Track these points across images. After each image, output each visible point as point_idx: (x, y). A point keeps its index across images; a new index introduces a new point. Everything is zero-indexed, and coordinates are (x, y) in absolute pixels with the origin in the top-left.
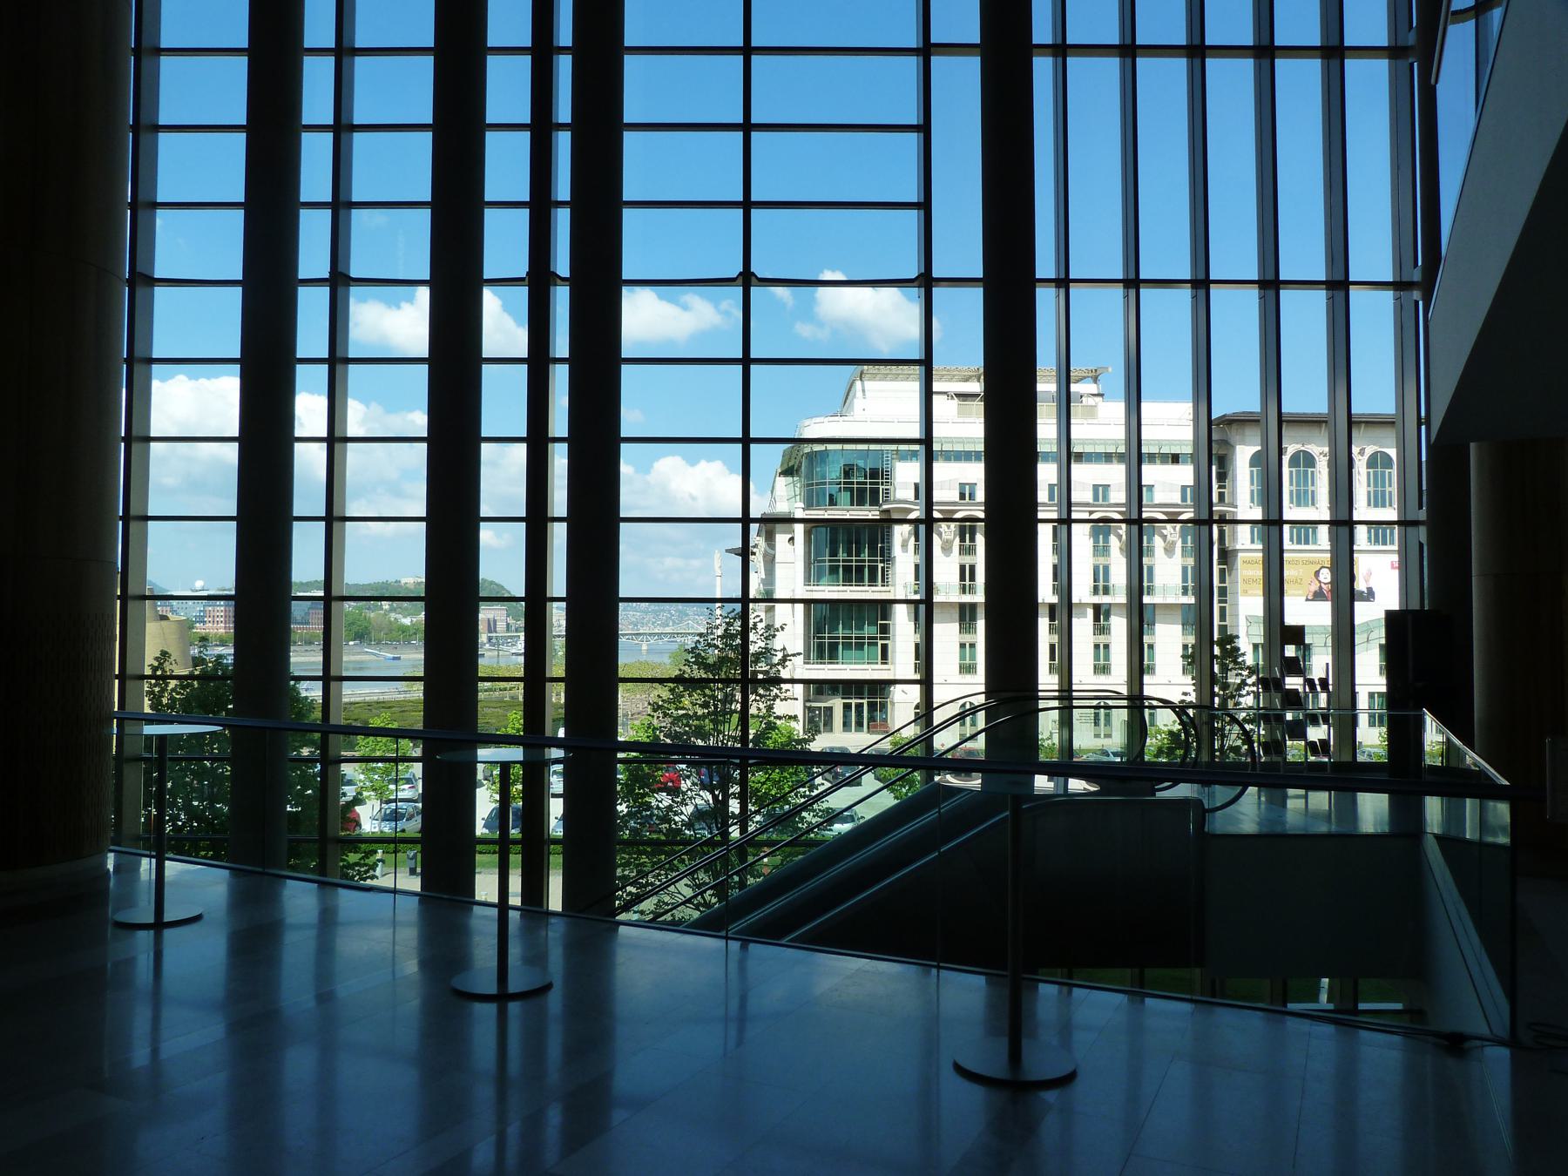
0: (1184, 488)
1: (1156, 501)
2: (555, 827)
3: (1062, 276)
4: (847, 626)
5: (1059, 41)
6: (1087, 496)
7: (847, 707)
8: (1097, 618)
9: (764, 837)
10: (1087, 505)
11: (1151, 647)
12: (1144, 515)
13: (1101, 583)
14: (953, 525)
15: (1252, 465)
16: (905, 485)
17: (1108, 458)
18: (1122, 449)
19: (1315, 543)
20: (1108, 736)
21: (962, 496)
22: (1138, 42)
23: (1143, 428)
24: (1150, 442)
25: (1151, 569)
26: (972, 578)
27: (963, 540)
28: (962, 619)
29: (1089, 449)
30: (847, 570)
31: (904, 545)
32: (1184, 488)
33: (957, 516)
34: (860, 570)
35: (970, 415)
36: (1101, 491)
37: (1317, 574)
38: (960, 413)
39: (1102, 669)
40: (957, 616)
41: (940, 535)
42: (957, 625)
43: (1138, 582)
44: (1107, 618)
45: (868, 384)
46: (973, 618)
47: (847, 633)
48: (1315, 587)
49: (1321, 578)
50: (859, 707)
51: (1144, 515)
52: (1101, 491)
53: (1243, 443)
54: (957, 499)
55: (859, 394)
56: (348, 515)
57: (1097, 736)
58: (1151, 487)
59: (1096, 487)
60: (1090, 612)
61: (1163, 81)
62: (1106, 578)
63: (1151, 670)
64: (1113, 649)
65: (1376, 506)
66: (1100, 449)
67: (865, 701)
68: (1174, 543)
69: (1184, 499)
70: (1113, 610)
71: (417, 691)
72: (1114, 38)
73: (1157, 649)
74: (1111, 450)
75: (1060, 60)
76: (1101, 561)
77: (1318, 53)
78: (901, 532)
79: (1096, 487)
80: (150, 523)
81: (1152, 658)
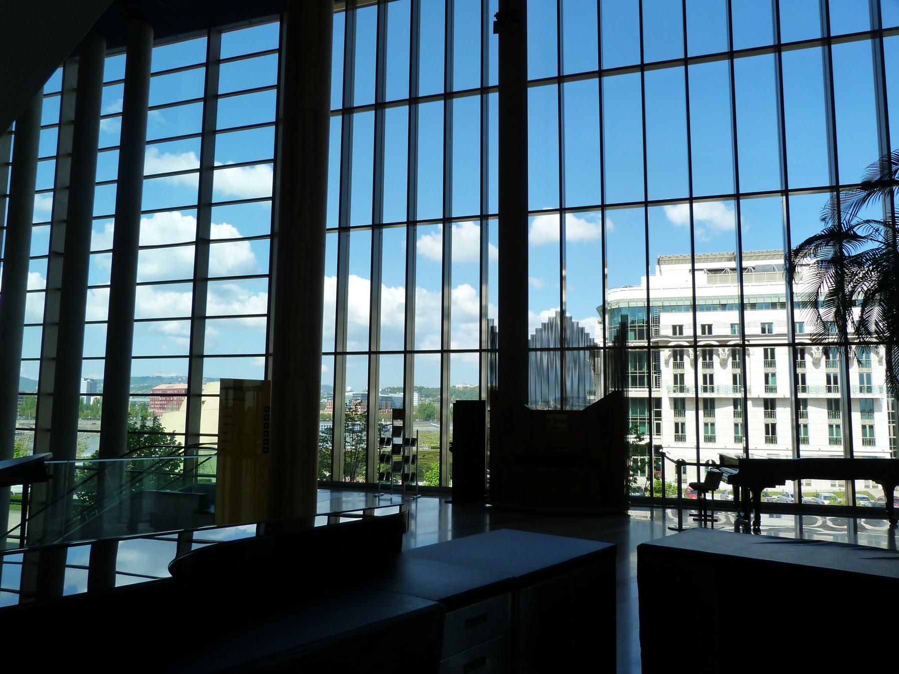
0: (732, 326)
3: (834, 184)
5: (826, 36)
6: (670, 332)
11: (805, 426)
12: (797, 341)
13: (866, 385)
14: (726, 349)
16: (666, 327)
17: (773, 305)
18: (783, 300)
21: (763, 331)
22: (884, 27)
23: (651, 291)
24: (702, 298)
25: (803, 376)
26: (836, 382)
27: (675, 359)
28: (766, 407)
29: (760, 301)
31: (667, 363)
32: (732, 326)
33: (729, 343)
34: (642, 378)
35: (775, 280)
36: (766, 329)
38: (709, 281)
39: (869, 441)
41: (718, 355)
42: (826, 411)
43: (798, 381)
44: (805, 407)
45: (663, 267)
46: (837, 409)
47: (634, 416)
51: (797, 341)
52: (678, 330)
54: (759, 332)
55: (658, 272)
56: (416, 349)
58: (801, 324)
59: (674, 327)
61: (804, 66)
62: (712, 382)
63: (806, 441)
64: (687, 426)
68: (819, 360)
69: (734, 331)
70: (809, 403)
71: (215, 440)
72: (818, 35)
73: (810, 428)
74: (775, 300)
75: (826, 47)
76: (679, 371)
77: (484, 96)
78: (665, 354)
79: (674, 327)
80: (381, 356)
81: (806, 433)
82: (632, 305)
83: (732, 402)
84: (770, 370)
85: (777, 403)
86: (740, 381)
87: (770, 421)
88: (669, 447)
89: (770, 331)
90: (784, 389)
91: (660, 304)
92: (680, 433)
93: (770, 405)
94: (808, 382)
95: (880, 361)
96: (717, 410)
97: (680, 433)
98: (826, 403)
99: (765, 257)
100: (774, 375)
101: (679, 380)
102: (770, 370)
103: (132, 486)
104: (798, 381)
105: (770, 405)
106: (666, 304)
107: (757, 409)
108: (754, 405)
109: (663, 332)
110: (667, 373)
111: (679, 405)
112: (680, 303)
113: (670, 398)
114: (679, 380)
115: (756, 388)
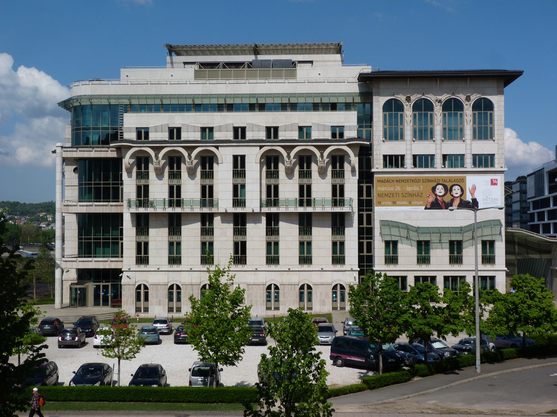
1: (313, 138)
2: (439, 388)
4: (97, 231)
6: (133, 136)
7: (97, 289)
8: (268, 223)
9: (215, 383)
10: (262, 141)
15: (384, 111)
17: (348, 106)
19: (432, 166)
20: (277, 308)
28: (236, 224)
30: (98, 190)
37: (434, 189)
40: (330, 223)
42: (297, 226)
43: (272, 194)
44: (277, 223)
48: (431, 199)
49: (454, 192)
50: (106, 287)
53: (379, 95)
57: (268, 308)
60: (264, 219)
62: (179, 195)
65: (480, 138)
66: (214, 101)
67: (109, 284)
70: (281, 217)
74: (350, 100)
82: (95, 102)
83: (199, 218)
84: (239, 181)
85: (248, 219)
86: (207, 193)
87: (240, 238)
88: (129, 270)
89: (341, 135)
90: (253, 202)
91: (126, 102)
92: (143, 255)
93: (240, 221)
94: (314, 195)
95: (353, 170)
96: (183, 228)
97: (143, 255)
98: (297, 218)
99: (235, 52)
100: (243, 186)
101: (143, 192)
102: (239, 181)
103: (432, 314)
104: (272, 194)
105: (240, 221)
106: (166, 102)
107: (226, 225)
108: (223, 221)
109: (126, 136)
110: (129, 186)
111: (142, 223)
112: (150, 102)
113: (132, 214)
114: (143, 192)
115: (224, 201)
